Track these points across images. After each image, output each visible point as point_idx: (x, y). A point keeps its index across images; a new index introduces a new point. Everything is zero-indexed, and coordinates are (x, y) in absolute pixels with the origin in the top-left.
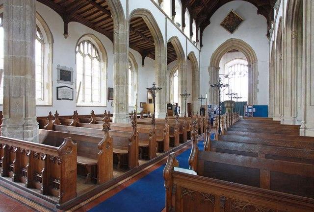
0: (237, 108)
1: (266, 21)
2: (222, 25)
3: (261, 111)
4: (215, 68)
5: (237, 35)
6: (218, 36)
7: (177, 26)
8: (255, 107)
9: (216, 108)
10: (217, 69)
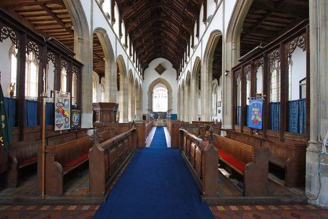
0: (163, 115)
1: (176, 72)
2: (155, 69)
3: (174, 117)
4: (151, 93)
5: (163, 76)
6: (152, 75)
7: (107, 17)
8: (171, 115)
9: (152, 115)
10: (152, 93)
